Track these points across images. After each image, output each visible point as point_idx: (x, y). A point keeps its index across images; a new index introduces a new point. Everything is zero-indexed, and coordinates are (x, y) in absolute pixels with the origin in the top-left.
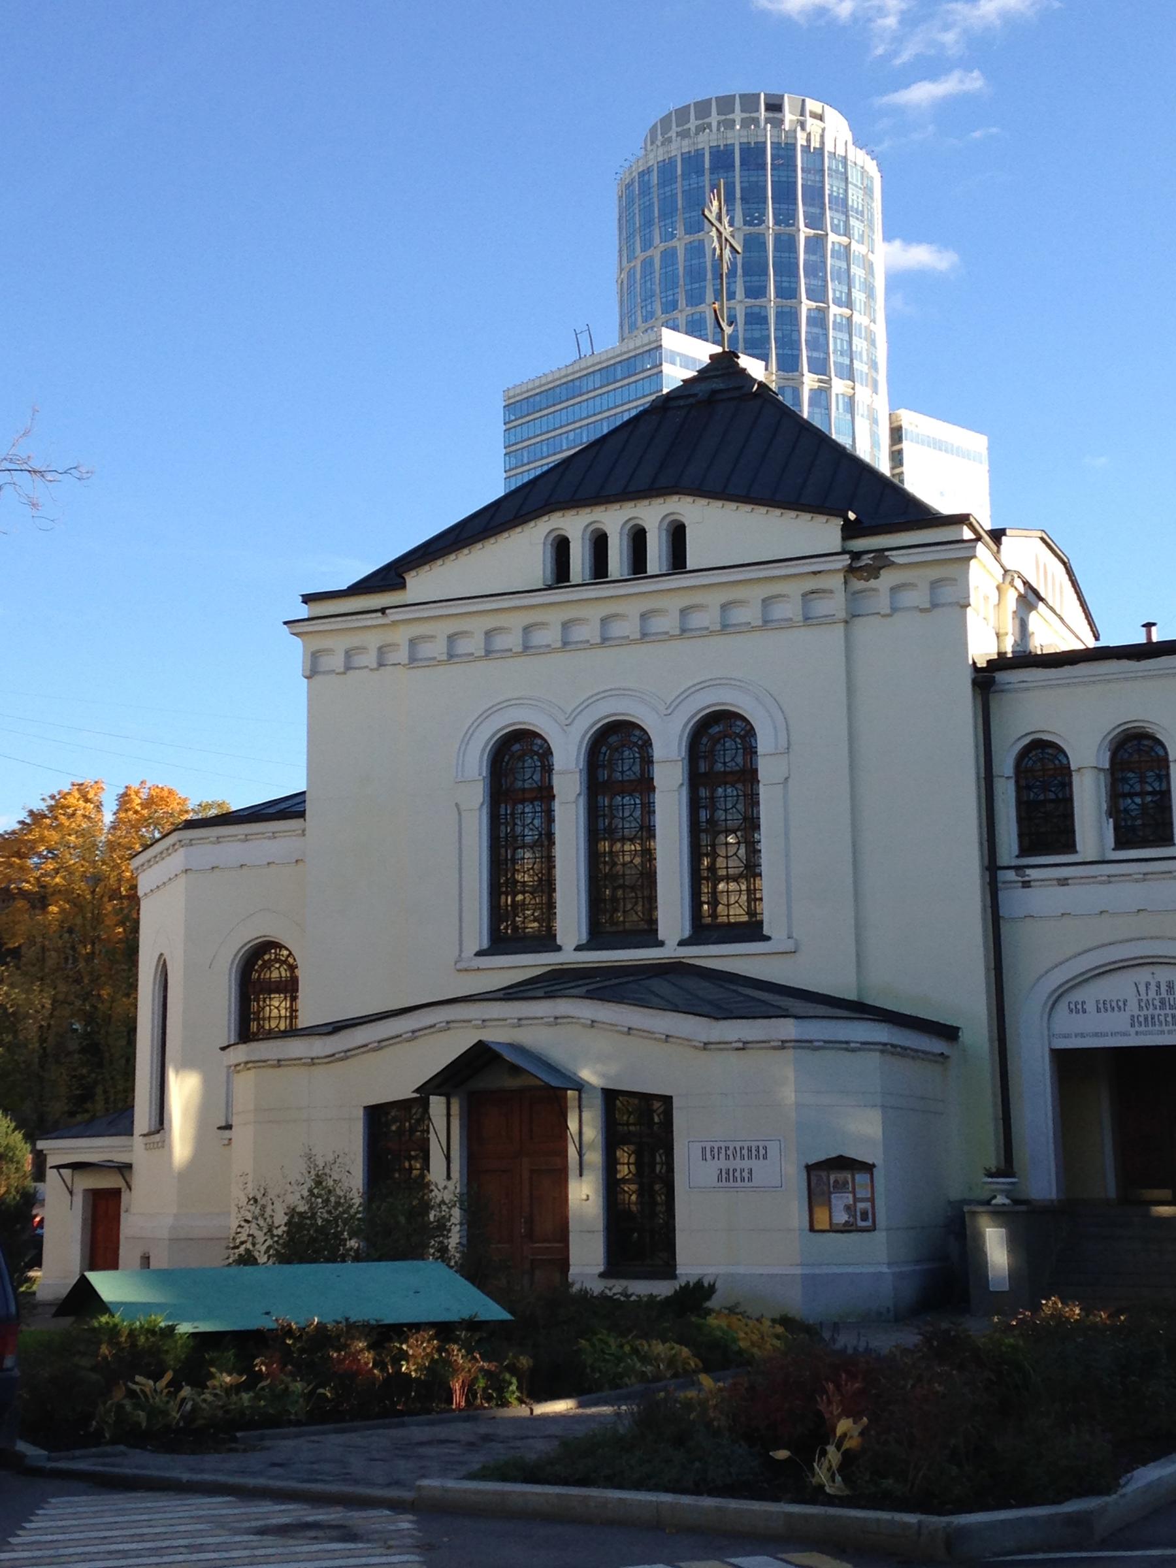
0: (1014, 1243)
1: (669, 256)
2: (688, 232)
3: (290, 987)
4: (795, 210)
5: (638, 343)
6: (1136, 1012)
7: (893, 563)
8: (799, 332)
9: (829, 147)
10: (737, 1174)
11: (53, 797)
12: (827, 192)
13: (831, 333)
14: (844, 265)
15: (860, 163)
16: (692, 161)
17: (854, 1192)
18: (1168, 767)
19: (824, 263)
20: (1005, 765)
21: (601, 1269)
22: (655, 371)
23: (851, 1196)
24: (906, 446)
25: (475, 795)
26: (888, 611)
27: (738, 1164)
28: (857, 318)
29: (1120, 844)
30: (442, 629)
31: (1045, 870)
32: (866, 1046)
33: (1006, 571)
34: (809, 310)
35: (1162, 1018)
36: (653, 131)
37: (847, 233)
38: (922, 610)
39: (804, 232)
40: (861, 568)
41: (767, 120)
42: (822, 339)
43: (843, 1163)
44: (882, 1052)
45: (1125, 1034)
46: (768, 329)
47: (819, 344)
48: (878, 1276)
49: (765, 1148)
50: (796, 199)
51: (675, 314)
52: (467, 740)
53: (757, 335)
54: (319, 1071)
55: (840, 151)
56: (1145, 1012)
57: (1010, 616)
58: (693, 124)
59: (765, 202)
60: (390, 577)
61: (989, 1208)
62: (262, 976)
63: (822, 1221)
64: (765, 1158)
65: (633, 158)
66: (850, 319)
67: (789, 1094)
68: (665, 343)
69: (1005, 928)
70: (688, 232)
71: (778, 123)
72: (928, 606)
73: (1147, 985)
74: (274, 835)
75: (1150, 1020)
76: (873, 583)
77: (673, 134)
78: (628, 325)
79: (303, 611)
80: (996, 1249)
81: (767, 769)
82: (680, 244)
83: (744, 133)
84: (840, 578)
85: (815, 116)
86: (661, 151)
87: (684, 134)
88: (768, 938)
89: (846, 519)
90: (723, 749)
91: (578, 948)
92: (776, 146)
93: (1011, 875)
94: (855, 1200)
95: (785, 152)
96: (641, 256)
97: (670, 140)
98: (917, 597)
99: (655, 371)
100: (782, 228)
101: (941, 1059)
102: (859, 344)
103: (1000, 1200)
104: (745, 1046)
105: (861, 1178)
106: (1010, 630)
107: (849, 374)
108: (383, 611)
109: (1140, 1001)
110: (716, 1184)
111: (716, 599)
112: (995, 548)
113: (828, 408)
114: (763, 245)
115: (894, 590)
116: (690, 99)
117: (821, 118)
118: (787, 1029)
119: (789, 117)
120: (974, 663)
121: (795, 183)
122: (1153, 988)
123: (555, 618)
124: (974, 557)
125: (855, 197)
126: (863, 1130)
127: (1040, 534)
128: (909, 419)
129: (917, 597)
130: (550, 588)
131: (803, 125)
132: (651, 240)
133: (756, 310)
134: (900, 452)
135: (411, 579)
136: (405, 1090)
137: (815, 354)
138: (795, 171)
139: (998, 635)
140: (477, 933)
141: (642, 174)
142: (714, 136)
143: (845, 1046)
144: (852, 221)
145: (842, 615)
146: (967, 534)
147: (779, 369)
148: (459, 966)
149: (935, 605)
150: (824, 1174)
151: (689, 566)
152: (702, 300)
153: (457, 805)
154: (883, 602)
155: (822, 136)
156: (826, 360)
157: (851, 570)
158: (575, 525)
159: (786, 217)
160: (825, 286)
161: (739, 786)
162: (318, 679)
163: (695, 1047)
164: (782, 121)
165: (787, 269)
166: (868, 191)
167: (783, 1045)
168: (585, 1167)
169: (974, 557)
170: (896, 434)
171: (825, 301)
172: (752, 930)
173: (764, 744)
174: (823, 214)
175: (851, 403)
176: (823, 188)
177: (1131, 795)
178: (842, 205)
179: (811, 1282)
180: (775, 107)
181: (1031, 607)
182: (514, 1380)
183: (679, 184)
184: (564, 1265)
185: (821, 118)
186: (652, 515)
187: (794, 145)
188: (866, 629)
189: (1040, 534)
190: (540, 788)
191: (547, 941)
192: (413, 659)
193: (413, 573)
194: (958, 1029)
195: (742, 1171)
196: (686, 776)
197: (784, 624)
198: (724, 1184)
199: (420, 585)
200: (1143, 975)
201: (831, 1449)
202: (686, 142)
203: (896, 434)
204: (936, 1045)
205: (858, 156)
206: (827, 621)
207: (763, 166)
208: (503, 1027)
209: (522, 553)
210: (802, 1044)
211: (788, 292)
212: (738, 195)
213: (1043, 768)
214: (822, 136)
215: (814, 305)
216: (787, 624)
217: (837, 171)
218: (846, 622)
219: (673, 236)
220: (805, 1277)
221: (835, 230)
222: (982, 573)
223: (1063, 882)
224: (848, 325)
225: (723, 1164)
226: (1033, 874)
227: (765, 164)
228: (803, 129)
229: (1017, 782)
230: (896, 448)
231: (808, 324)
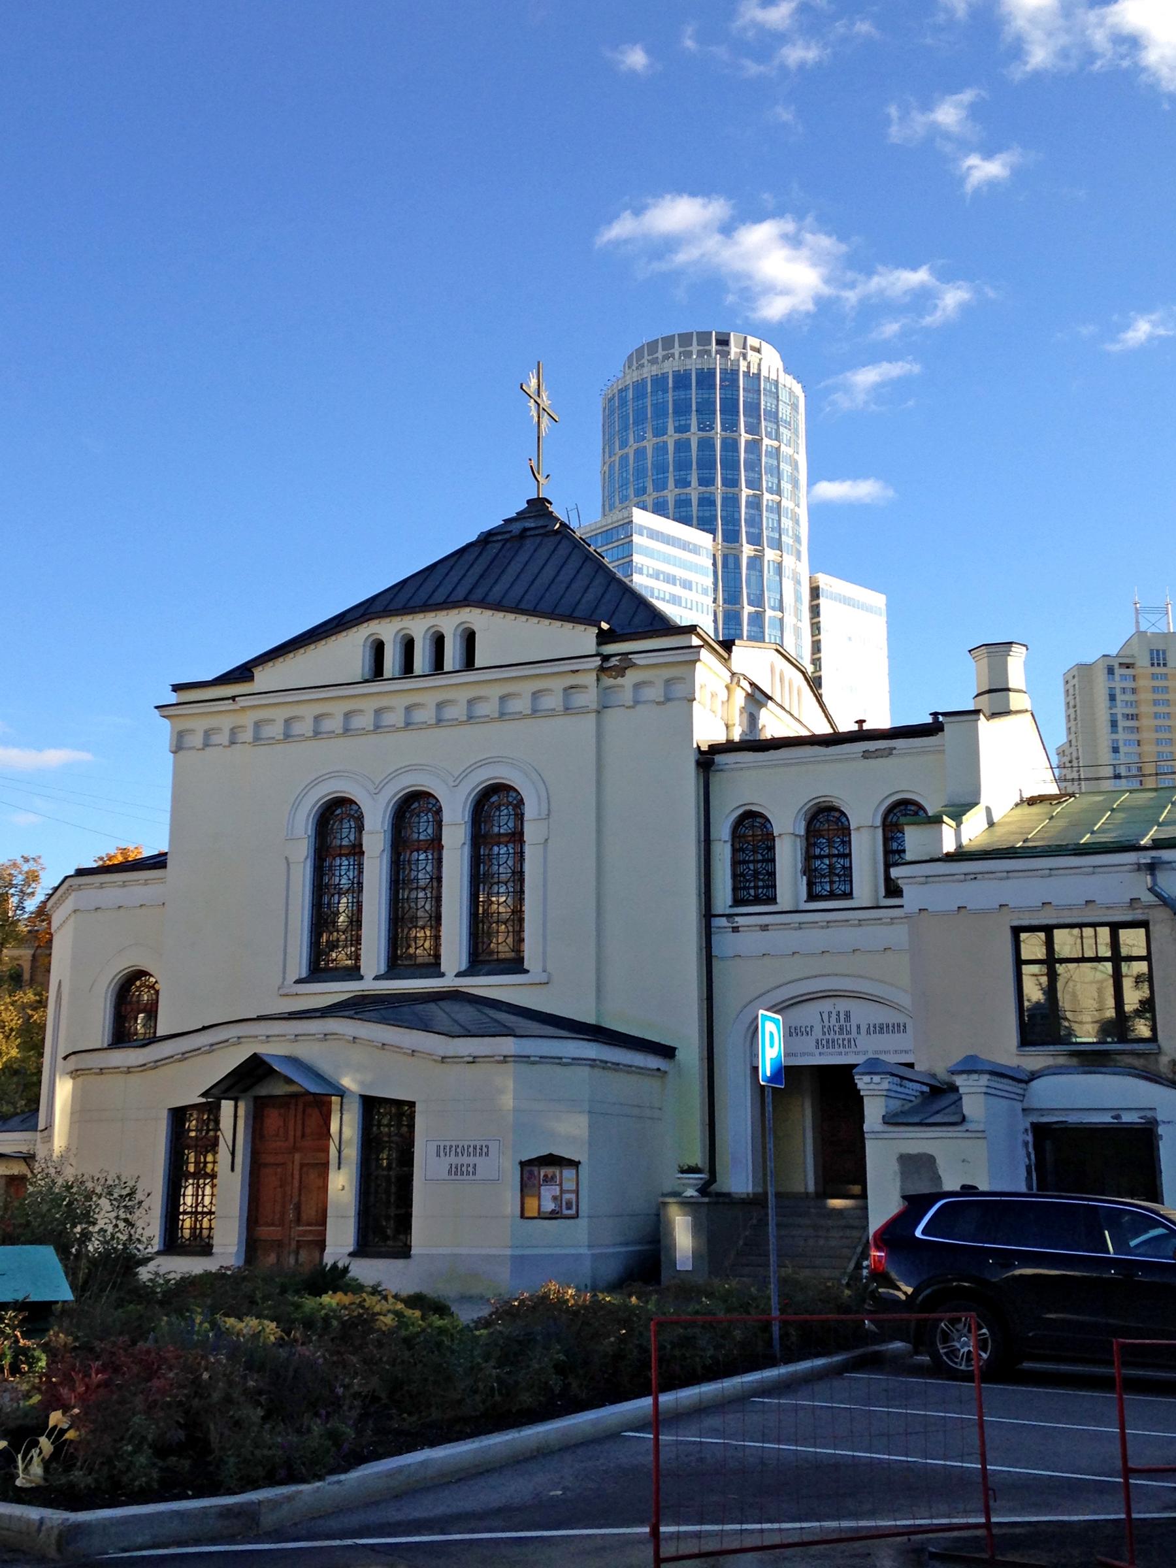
0: (697, 1229)
1: (640, 453)
2: (656, 435)
3: (152, 1011)
4: (738, 421)
5: (615, 519)
6: (820, 1036)
7: (634, 665)
8: (739, 512)
9: (764, 373)
10: (464, 1169)
11: (101, 859)
12: (762, 407)
13: (765, 513)
14: (775, 463)
15: (788, 385)
16: (659, 382)
17: (561, 1185)
18: (850, 834)
19: (760, 460)
20: (722, 831)
21: (351, 1249)
22: (627, 540)
23: (558, 1188)
24: (822, 601)
25: (302, 851)
26: (631, 703)
27: (465, 1160)
28: (785, 503)
29: (812, 897)
30: (281, 714)
31: (750, 918)
32: (576, 1061)
33: (733, 674)
34: (748, 496)
35: (840, 1042)
36: (630, 357)
37: (777, 438)
38: (658, 703)
39: (744, 437)
40: (608, 668)
41: (717, 352)
42: (757, 518)
44: (591, 1066)
45: (812, 1055)
46: (716, 510)
47: (755, 522)
48: (578, 1257)
49: (487, 1147)
50: (738, 412)
51: (645, 498)
52: (296, 805)
53: (707, 514)
54: (134, 1079)
55: (773, 376)
56: (827, 1036)
57: (737, 713)
58: (660, 353)
59: (715, 413)
60: (243, 673)
61: (679, 1199)
62: (131, 1007)
63: (532, 1211)
64: (487, 1154)
65: (614, 379)
66: (779, 503)
67: (508, 1101)
68: (635, 520)
69: (717, 966)
70: (656, 435)
72: (662, 699)
73: (830, 1013)
74: (146, 882)
75: (831, 1043)
76: (620, 680)
77: (645, 361)
78: (608, 505)
79: (173, 698)
80: (683, 1237)
81: (531, 832)
83: (699, 361)
84: (593, 676)
86: (635, 374)
87: (654, 362)
88: (527, 971)
89: (600, 629)
90: (495, 808)
91: (377, 978)
93: (723, 922)
94: (562, 1191)
95: (731, 376)
97: (642, 366)
98: (654, 693)
99: (627, 540)
100: (728, 434)
101: (658, 1074)
102: (786, 523)
103: (691, 1192)
104: (474, 1060)
105: (568, 1173)
106: (737, 721)
107: (778, 545)
108: (233, 698)
109: (823, 1027)
110: (446, 1176)
111: (496, 692)
112: (726, 656)
113: (761, 571)
114: (712, 447)
115: (637, 686)
117: (758, 351)
118: (508, 1045)
119: (734, 350)
120: (699, 747)
121: (738, 400)
122: (834, 1016)
123: (369, 706)
124: (699, 660)
125: (784, 411)
126: (569, 1132)
127: (774, 646)
128: (824, 580)
130: (366, 681)
131: (745, 357)
132: (627, 441)
133: (707, 495)
134: (818, 606)
135: (258, 673)
136: (194, 1098)
137: (752, 530)
138: (738, 391)
139: (727, 726)
141: (621, 391)
142: (676, 363)
144: (782, 429)
145: (594, 706)
146: (696, 641)
147: (724, 541)
148: (281, 992)
149: (668, 699)
150: (535, 1169)
151: (477, 666)
152: (665, 488)
153: (286, 858)
154: (627, 696)
155: (759, 365)
156: (760, 535)
157: (602, 669)
158: (388, 630)
159: (731, 425)
160: (761, 479)
161: (511, 845)
162: (181, 753)
163: (435, 1061)
164: (729, 353)
165: (731, 465)
166: (795, 407)
167: (505, 1059)
168: (343, 1161)
169: (699, 660)
170: (815, 592)
171: (760, 488)
172: (515, 965)
173: (530, 811)
174: (759, 423)
175: (779, 568)
176: (759, 404)
177: (821, 857)
178: (774, 417)
179: (520, 1262)
180: (723, 342)
181: (761, 705)
182: (44, 1357)
183: (649, 400)
184: (321, 1245)
185: (758, 351)
186: (449, 622)
187: (738, 370)
188: (613, 717)
189: (774, 646)
190: (354, 846)
191: (353, 973)
192: (257, 738)
193: (260, 668)
194: (674, 1049)
195: (469, 1165)
196: (469, 838)
197: (550, 713)
198: (453, 1177)
199: (264, 678)
200: (826, 1005)
201: (43, 1440)
202: (654, 368)
203: (815, 592)
204: (653, 1062)
205: (787, 381)
206: (583, 711)
208: (274, 1045)
209: (348, 652)
210: (593, 1063)
211: (732, 482)
212: (694, 408)
213: (753, 832)
214: (759, 365)
215: (751, 492)
216: (551, 714)
217: (770, 391)
218: (598, 712)
219: (644, 438)
220: (514, 1258)
221: (769, 435)
222: (709, 672)
223: (764, 928)
224: (778, 508)
225: (453, 1159)
226: (740, 921)
227: (715, 385)
228: (745, 358)
229: (732, 845)
230: (815, 603)
231: (747, 507)
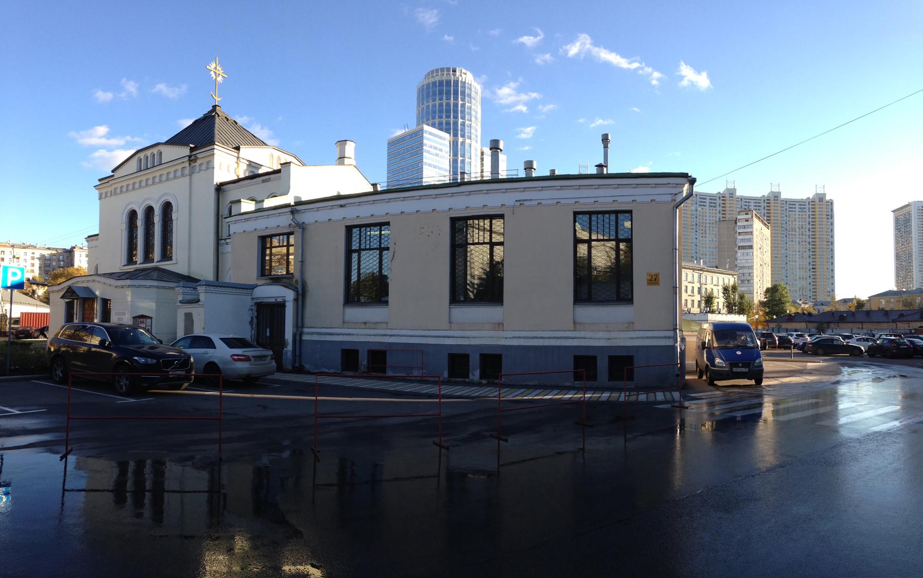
1: (428, 107)
16: (434, 83)
32: (150, 286)
43: (143, 317)
47: (463, 130)
71: (455, 75)
78: (418, 124)
82: (431, 104)
90: (167, 208)
95: (456, 82)
102: (473, 131)
107: (470, 138)
116: (434, 68)
119: (458, 73)
125: (473, 94)
129: (204, 167)
140: (124, 261)
143: (145, 286)
159: (456, 99)
165: (456, 112)
178: (470, 96)
180: (454, 71)
188: (195, 176)
210: (158, 287)
211: (456, 117)
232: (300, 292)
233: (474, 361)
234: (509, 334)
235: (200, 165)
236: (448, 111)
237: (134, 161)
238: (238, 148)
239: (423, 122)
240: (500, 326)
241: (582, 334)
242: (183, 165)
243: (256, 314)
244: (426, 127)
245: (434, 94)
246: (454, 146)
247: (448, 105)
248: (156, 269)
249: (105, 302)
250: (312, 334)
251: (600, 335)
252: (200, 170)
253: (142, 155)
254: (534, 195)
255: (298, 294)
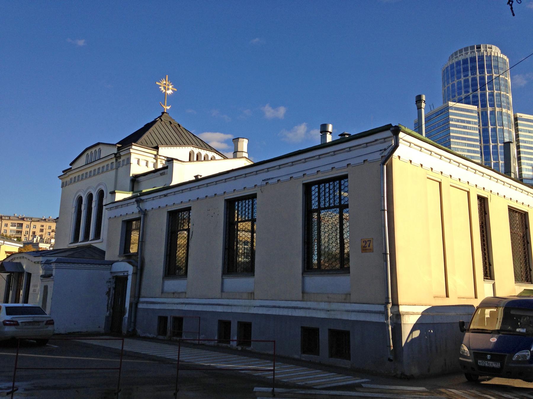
1: (453, 85)
9: (493, 54)
16: (458, 63)
82: (456, 82)
85: (489, 48)
92: (479, 56)
95: (481, 58)
96: (447, 86)
107: (500, 106)
114: (476, 80)
116: (457, 49)
131: (486, 51)
141: (446, 68)
164: (481, 51)
178: (497, 67)
180: (479, 47)
185: (491, 48)
188: (120, 169)
207: (476, 61)
232: (139, 268)
233: (324, 338)
234: (258, 303)
235: (123, 161)
236: (474, 85)
237: (84, 157)
238: (157, 148)
239: (449, 100)
240: (251, 295)
241: (309, 304)
242: (111, 161)
243: (114, 286)
244: (451, 104)
245: (459, 72)
246: (483, 118)
247: (474, 79)
248: (90, 247)
249: (29, 275)
250: (147, 303)
251: (323, 305)
252: (123, 165)
253: (89, 152)
254: (201, 193)
255: (137, 269)
